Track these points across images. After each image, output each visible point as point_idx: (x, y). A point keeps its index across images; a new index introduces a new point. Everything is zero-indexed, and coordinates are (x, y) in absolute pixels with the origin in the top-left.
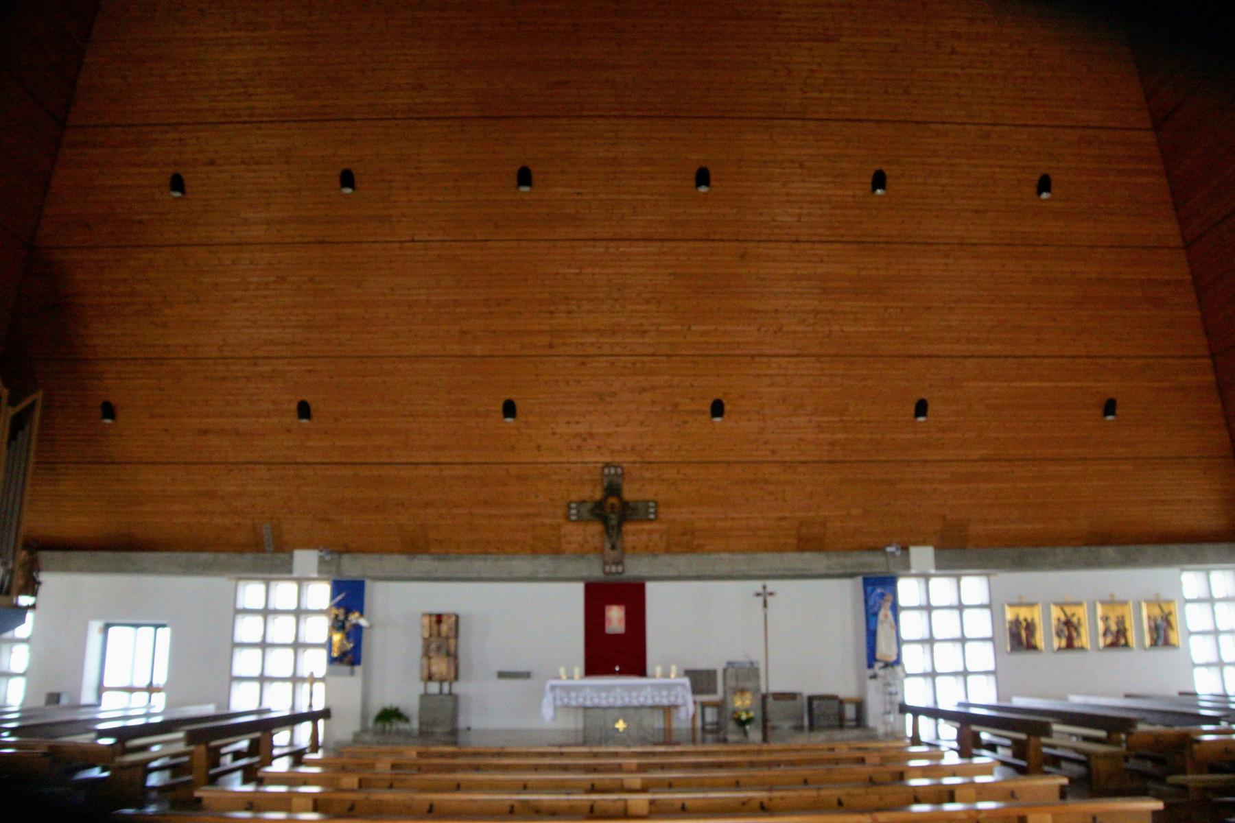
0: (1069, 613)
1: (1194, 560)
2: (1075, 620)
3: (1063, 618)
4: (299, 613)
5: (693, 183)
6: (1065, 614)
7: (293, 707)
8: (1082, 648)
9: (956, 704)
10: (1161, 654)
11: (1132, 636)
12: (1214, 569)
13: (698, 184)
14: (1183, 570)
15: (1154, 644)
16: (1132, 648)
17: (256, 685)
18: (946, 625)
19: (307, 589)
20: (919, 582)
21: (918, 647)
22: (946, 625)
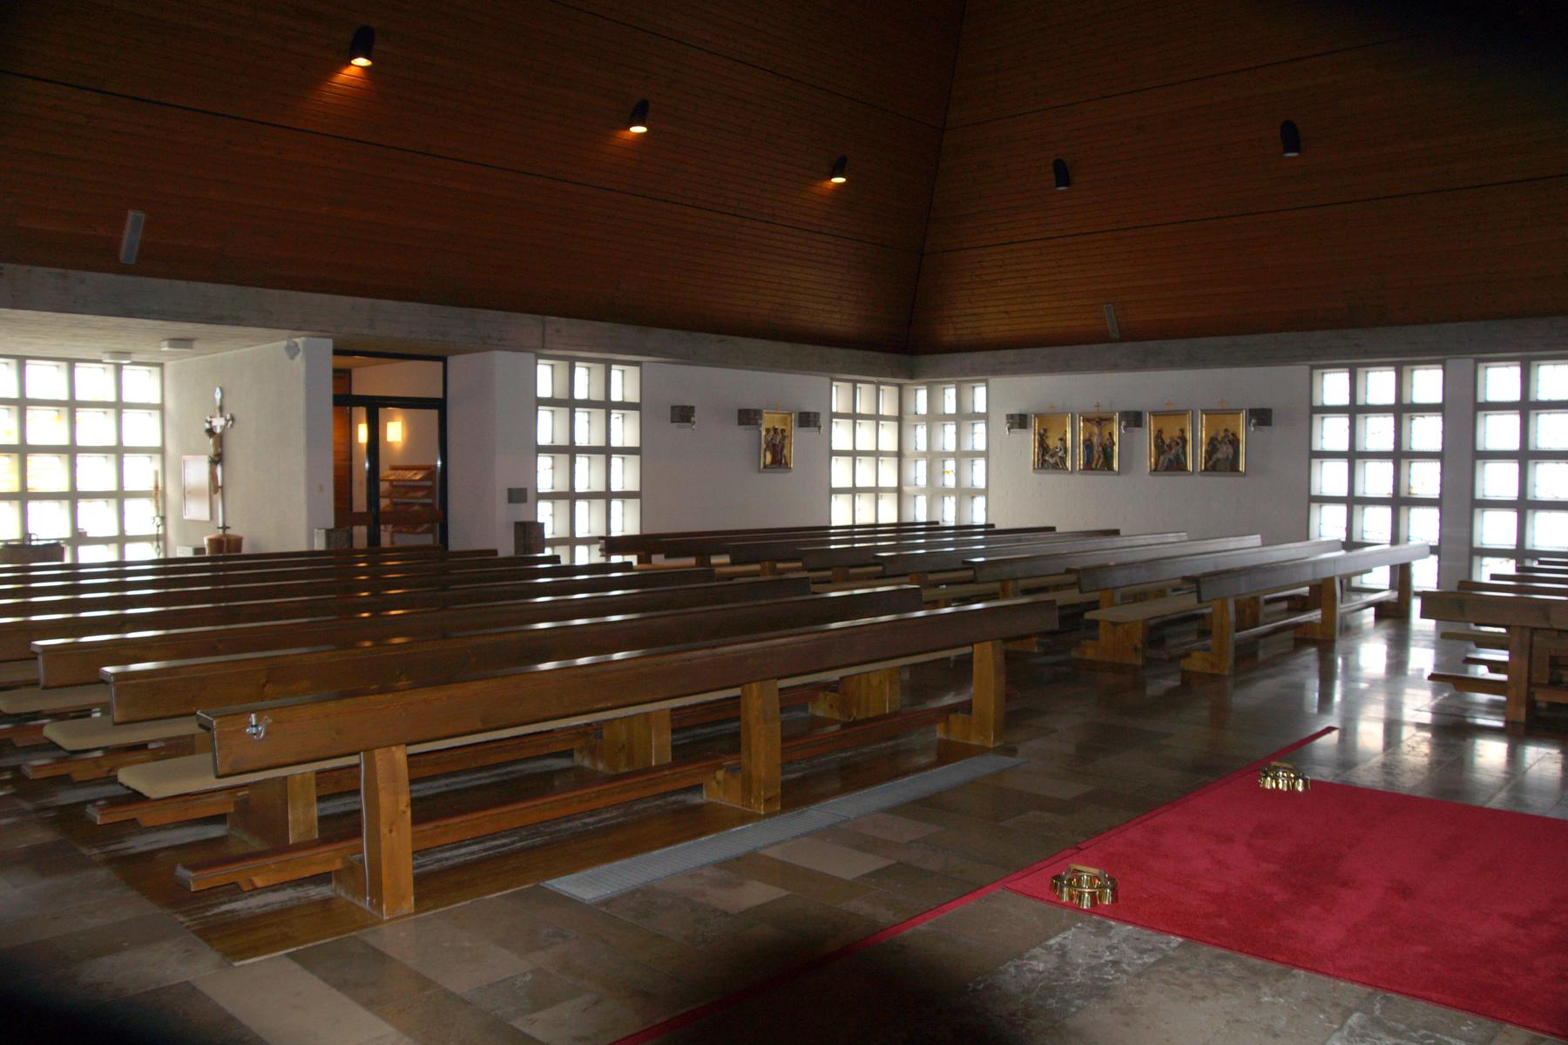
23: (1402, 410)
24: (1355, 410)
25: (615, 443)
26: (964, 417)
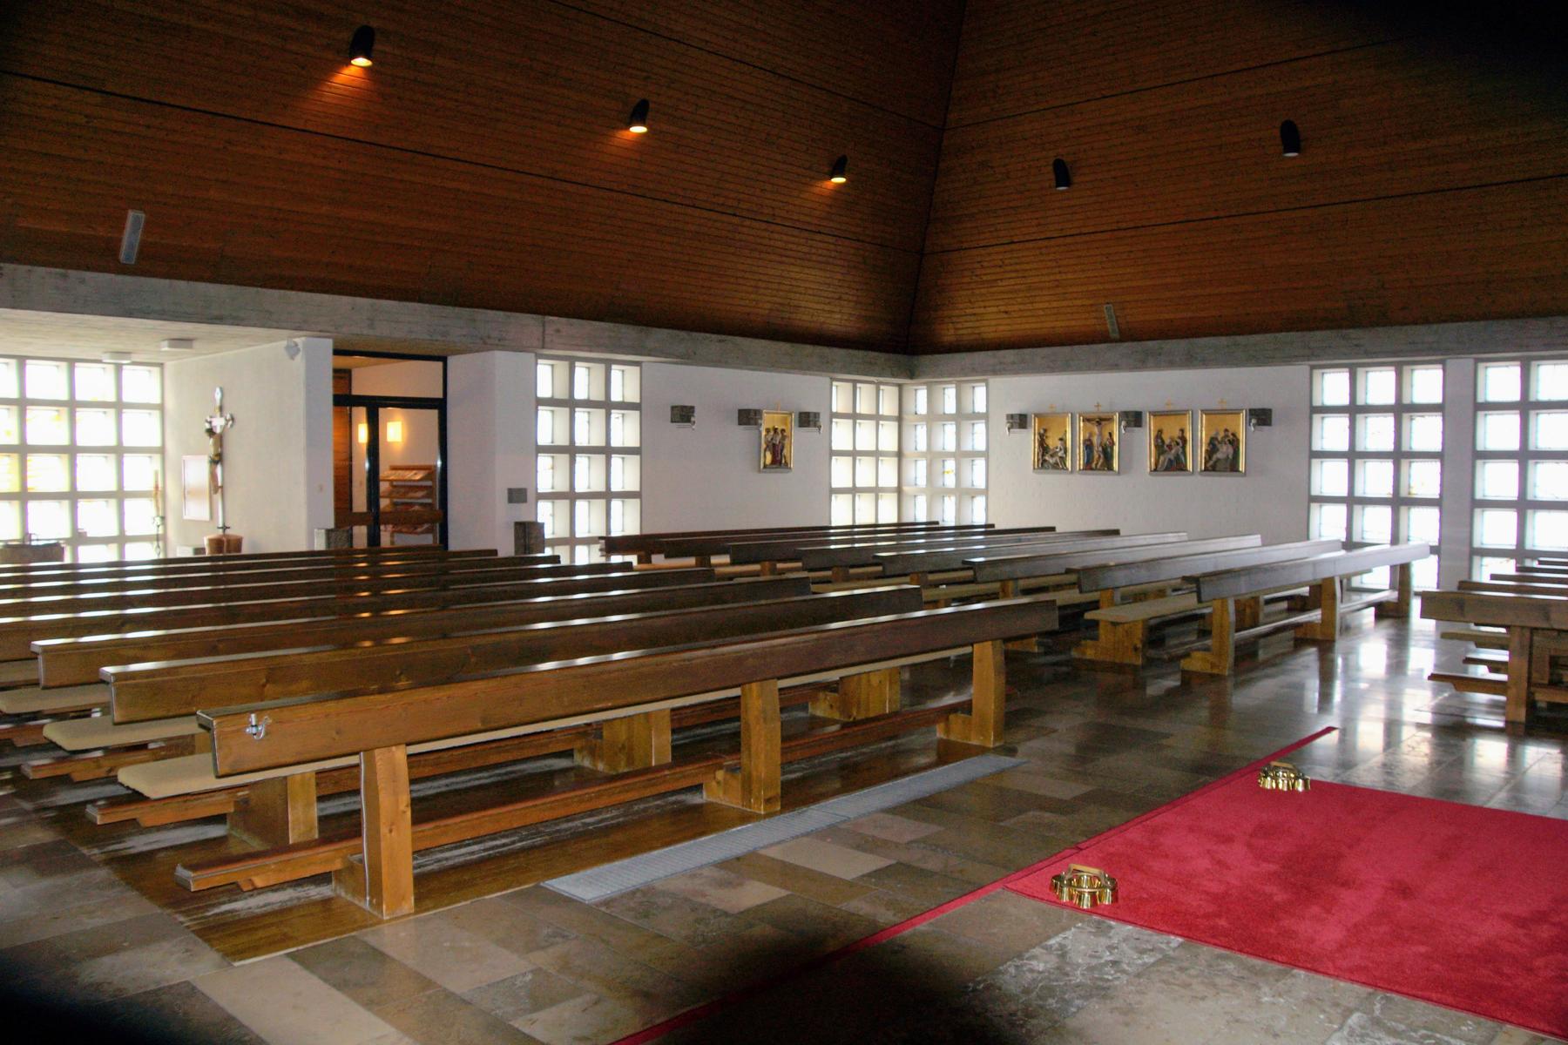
1: (830, 369)
23: (1402, 410)
24: (1354, 410)
25: (616, 396)
26: (963, 417)
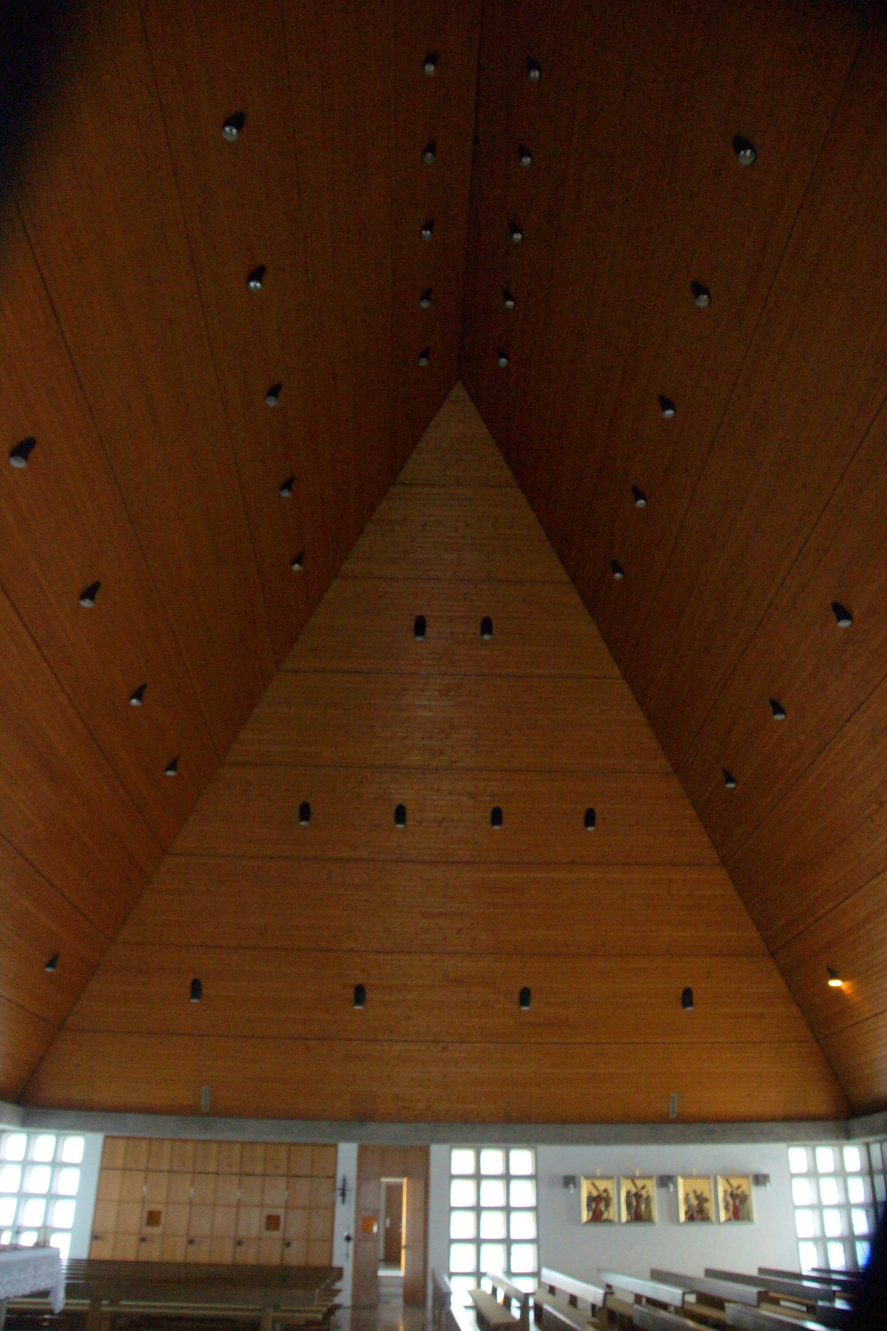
0: (601, 1188)
1: (792, 1139)
2: (644, 1193)
3: (729, 1190)
4: (56, 1164)
5: (478, 632)
6: (597, 1189)
7: (282, 1261)
8: (608, 1221)
9: (811, 1269)
10: (739, 1229)
11: (710, 1207)
12: (845, 1144)
13: (483, 633)
14: (789, 1146)
15: (691, 1218)
16: (711, 1221)
17: (483, 1236)
18: (492, 1193)
19: (63, 1143)
20: (806, 1150)
21: (809, 1212)
22: (492, 1193)
